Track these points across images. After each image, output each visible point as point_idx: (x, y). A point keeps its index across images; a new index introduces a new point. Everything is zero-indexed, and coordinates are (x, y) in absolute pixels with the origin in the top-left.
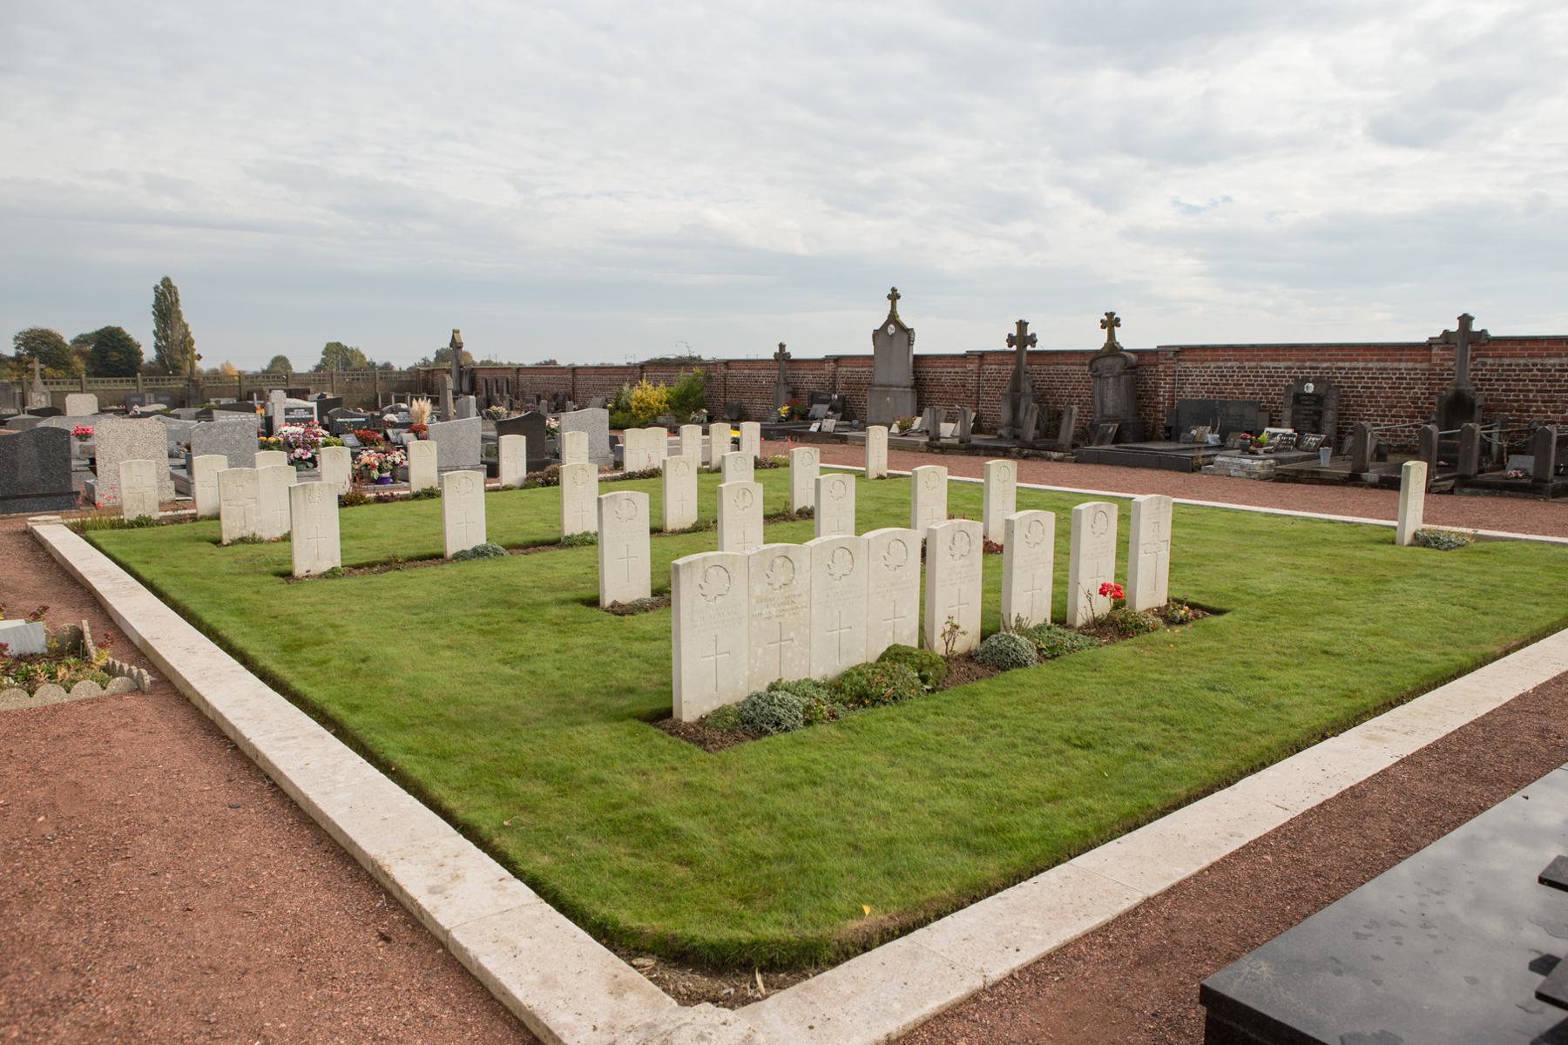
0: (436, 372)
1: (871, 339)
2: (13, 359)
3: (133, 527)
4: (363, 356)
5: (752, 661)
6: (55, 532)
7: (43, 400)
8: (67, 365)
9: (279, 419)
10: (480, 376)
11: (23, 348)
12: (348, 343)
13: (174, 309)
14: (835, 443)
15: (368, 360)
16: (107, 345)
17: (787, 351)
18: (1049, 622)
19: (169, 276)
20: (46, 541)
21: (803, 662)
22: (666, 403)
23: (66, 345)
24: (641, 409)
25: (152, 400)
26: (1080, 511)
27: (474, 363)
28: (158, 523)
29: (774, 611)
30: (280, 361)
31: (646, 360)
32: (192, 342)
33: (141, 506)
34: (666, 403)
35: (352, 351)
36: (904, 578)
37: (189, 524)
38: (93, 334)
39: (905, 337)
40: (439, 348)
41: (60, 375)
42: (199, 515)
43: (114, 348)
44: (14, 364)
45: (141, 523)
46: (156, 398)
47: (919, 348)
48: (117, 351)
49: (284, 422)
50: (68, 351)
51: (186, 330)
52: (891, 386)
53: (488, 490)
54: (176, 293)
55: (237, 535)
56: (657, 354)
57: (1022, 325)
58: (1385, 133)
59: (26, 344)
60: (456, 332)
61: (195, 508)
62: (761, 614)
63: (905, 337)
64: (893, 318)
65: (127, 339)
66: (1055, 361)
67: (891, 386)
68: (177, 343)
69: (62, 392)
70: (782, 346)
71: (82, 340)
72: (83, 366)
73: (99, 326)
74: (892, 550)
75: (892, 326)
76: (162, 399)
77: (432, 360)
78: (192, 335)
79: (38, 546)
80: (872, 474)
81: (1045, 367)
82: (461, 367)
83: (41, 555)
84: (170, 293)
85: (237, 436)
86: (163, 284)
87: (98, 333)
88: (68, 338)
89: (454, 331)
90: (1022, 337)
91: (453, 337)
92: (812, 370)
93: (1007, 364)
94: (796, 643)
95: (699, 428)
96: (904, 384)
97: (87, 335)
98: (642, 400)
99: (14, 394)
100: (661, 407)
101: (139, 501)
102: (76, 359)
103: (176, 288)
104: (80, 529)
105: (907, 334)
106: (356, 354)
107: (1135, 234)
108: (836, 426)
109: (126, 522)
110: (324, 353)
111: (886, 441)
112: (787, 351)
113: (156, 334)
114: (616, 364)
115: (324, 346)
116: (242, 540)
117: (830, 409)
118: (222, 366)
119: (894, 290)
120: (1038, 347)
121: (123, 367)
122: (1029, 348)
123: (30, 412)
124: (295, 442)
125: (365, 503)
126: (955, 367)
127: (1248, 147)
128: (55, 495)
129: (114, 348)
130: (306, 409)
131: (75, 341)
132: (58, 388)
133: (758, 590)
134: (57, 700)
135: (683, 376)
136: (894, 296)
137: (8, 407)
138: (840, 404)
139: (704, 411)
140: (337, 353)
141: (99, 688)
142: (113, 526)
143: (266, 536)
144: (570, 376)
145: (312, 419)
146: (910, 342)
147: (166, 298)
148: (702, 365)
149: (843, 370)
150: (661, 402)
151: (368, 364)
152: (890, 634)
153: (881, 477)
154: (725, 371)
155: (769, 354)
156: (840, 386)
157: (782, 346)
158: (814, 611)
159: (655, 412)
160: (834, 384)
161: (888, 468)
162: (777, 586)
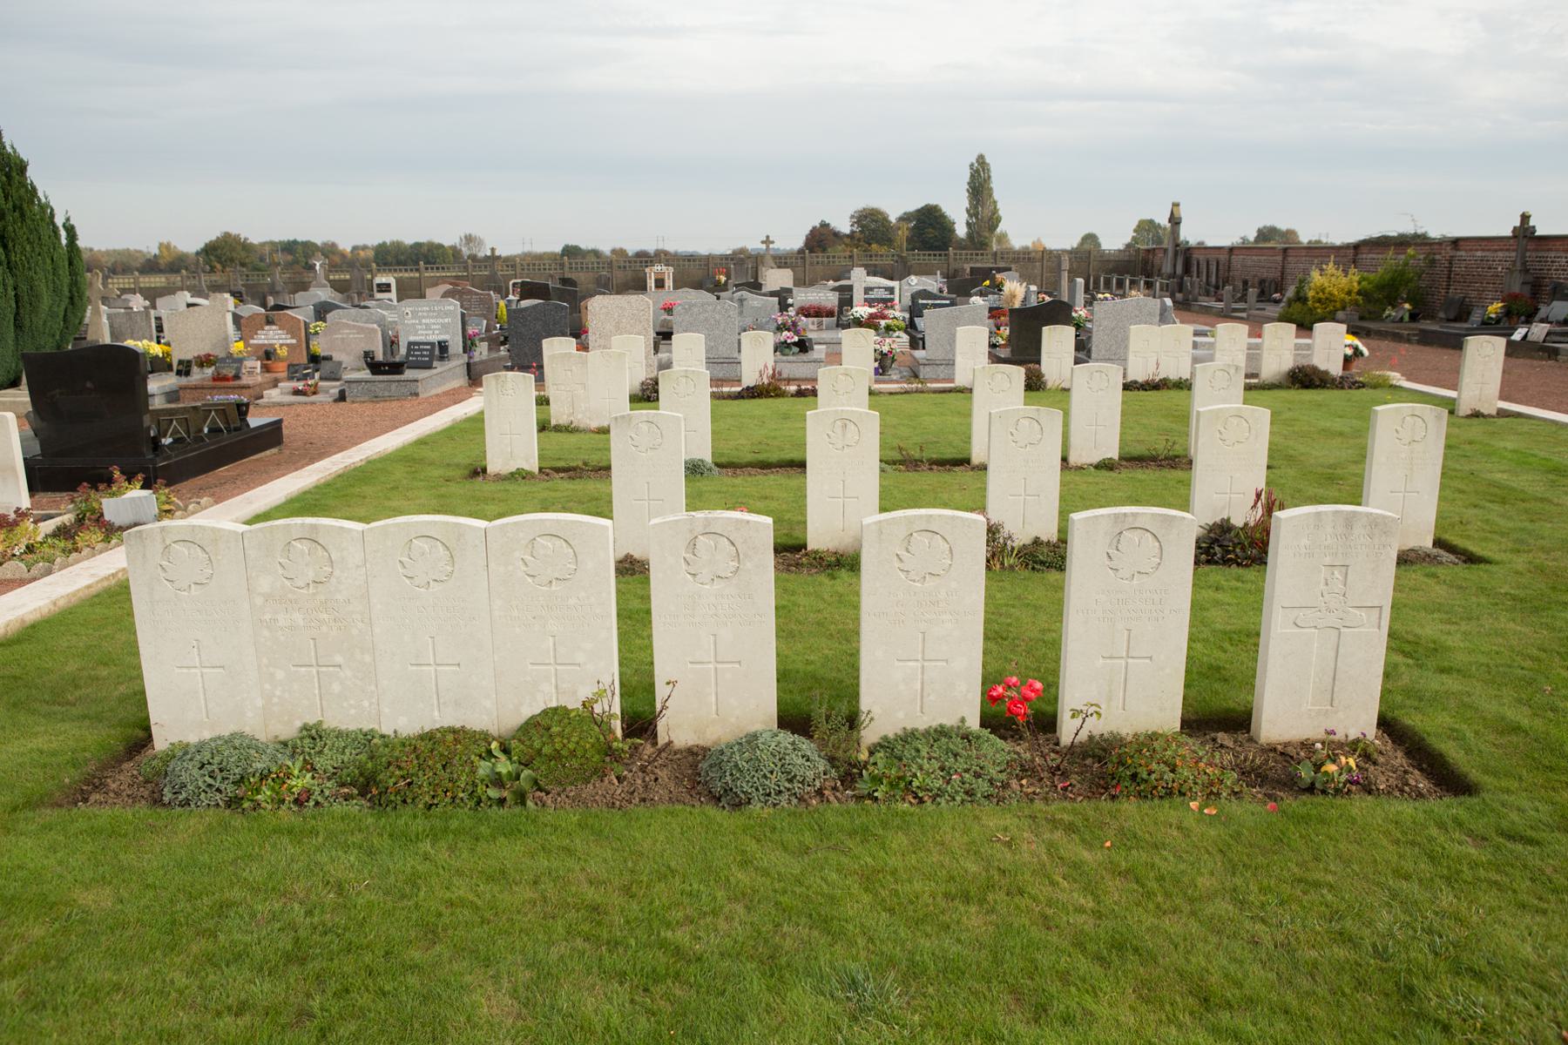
2: (847, 236)
5: (267, 686)
9: (858, 296)
10: (1195, 256)
14: (1542, 359)
17: (1531, 224)
18: (974, 723)
19: (984, 153)
21: (366, 704)
24: (1319, 301)
27: (1299, 242)
30: (1090, 238)
31: (1362, 238)
32: (999, 220)
34: (1359, 293)
36: (572, 602)
40: (1261, 226)
44: (847, 241)
48: (934, 228)
51: (995, 208)
53: (715, 396)
54: (988, 170)
56: (1374, 232)
60: (1176, 205)
62: (276, 620)
65: (943, 216)
68: (986, 219)
70: (1525, 218)
71: (905, 218)
73: (919, 206)
80: (1464, 409)
82: (1177, 245)
85: (717, 317)
86: (977, 161)
87: (918, 211)
97: (910, 213)
98: (1323, 290)
108: (1548, 334)
110: (1135, 231)
112: (1531, 224)
113: (968, 211)
115: (1136, 223)
118: (1033, 243)
130: (887, 289)
131: (901, 219)
133: (264, 584)
135: (1391, 259)
139: (1407, 306)
140: (1149, 230)
143: (1486, 413)
144: (1279, 258)
145: (892, 300)
147: (979, 175)
148: (1426, 244)
150: (1349, 293)
153: (1476, 415)
154: (1452, 253)
155: (1504, 227)
157: (1525, 218)
159: (1338, 305)
161: (1503, 397)
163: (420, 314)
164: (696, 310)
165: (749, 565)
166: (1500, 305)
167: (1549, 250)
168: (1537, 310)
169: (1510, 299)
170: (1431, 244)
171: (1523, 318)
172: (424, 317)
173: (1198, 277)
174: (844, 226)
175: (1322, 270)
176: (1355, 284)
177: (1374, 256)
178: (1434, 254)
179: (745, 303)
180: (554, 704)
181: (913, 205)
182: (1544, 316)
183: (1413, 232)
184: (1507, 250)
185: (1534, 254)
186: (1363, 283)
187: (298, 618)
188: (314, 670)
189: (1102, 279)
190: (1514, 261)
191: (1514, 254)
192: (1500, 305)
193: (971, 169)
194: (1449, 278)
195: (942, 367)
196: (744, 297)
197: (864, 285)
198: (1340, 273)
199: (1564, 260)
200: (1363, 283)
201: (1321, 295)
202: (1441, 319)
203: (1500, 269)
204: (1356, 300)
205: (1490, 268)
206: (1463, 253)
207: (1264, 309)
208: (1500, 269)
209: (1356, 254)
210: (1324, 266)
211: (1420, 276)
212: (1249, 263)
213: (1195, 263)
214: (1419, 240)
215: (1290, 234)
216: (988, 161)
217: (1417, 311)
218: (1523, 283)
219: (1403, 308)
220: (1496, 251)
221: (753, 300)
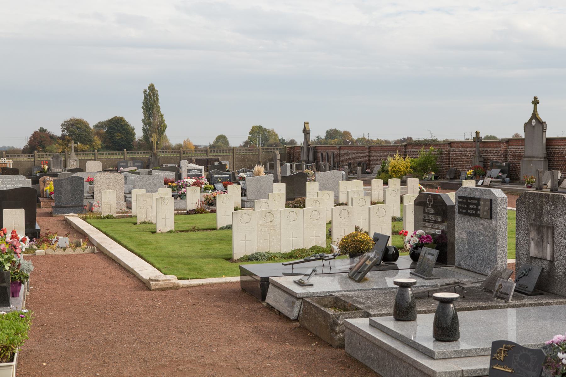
0: (296, 148)
1: (523, 129)
2: (60, 138)
3: (105, 219)
4: (276, 135)
5: (259, 244)
6: (76, 219)
7: (75, 164)
8: (90, 142)
9: (184, 174)
10: (320, 151)
11: (66, 131)
12: (267, 126)
15: (280, 137)
16: (114, 129)
21: (278, 247)
22: (411, 168)
23: (90, 129)
24: (394, 172)
25: (132, 165)
28: (116, 218)
29: (266, 229)
30: (222, 139)
32: (165, 127)
33: (109, 210)
34: (411, 168)
35: (269, 132)
36: (319, 224)
37: (128, 218)
38: (106, 121)
40: (328, 129)
41: (86, 148)
42: (133, 215)
43: (118, 130)
44: (60, 141)
45: (109, 217)
46: (133, 163)
47: (550, 133)
48: (120, 133)
49: (187, 177)
50: (91, 133)
51: (162, 119)
52: (534, 157)
54: (157, 94)
55: (143, 220)
59: (67, 129)
60: (306, 123)
61: (131, 213)
62: (262, 230)
64: (535, 116)
65: (127, 125)
67: (534, 157)
68: (156, 127)
69: (85, 160)
70: (477, 133)
71: (100, 126)
72: (100, 142)
74: (313, 214)
75: (534, 120)
76: (137, 164)
77: (323, 138)
79: (69, 224)
82: (309, 145)
83: (69, 227)
85: (155, 182)
87: (109, 121)
88: (92, 123)
89: (305, 123)
91: (305, 127)
92: (495, 148)
94: (275, 240)
95: (399, 180)
96: (541, 156)
98: (395, 167)
99: (61, 160)
100: (406, 170)
102: (96, 138)
104: (85, 219)
105: (542, 125)
106: (271, 133)
109: (103, 217)
110: (250, 133)
113: (143, 121)
114: (457, 140)
116: (144, 223)
118: (185, 142)
119: (535, 98)
121: (123, 143)
123: (68, 171)
124: (182, 185)
125: (205, 213)
128: (76, 207)
129: (118, 130)
131: (96, 126)
132: (83, 157)
133: (260, 222)
134: (71, 253)
135: (423, 152)
136: (536, 102)
137: (57, 168)
138: (507, 169)
139: (433, 173)
140: (259, 133)
141: (82, 251)
142: (97, 218)
144: (367, 151)
145: (201, 175)
146: (544, 130)
147: (150, 97)
148: (437, 145)
150: (407, 168)
151: (280, 140)
152: (313, 242)
155: (471, 137)
156: (509, 158)
157: (477, 133)
158: (282, 231)
159: (403, 173)
160: (506, 156)
162: (267, 222)
163: (6, 182)
164: (145, 179)
165: (351, 215)
166: (472, 171)
167: (488, 147)
168: (486, 172)
169: (475, 168)
170: (440, 144)
171: (481, 176)
172: (8, 184)
173: (328, 162)
174: (58, 132)
175: (394, 157)
176: (409, 164)
177: (414, 150)
178: (441, 149)
179: (128, 178)
180: (314, 245)
181: (106, 117)
182: (489, 175)
183: (431, 139)
184: (472, 147)
185: (483, 149)
186: (412, 163)
187: (266, 229)
188: (268, 240)
189: (268, 164)
190: (475, 152)
191: (475, 149)
192: (472, 171)
193: (145, 94)
194: (449, 160)
196: (127, 175)
197: (187, 168)
198: (402, 158)
199: (494, 151)
200: (412, 163)
202: (448, 178)
203: (470, 156)
204: (410, 171)
205: (466, 155)
206: (454, 149)
207: (366, 177)
208: (470, 156)
209: (405, 149)
210: (395, 156)
211: (436, 159)
212: (351, 154)
213: (320, 155)
214: (434, 143)
215: (347, 134)
216: (156, 88)
217: (437, 175)
218: (480, 162)
219: (431, 174)
220: (467, 147)
221: (132, 176)
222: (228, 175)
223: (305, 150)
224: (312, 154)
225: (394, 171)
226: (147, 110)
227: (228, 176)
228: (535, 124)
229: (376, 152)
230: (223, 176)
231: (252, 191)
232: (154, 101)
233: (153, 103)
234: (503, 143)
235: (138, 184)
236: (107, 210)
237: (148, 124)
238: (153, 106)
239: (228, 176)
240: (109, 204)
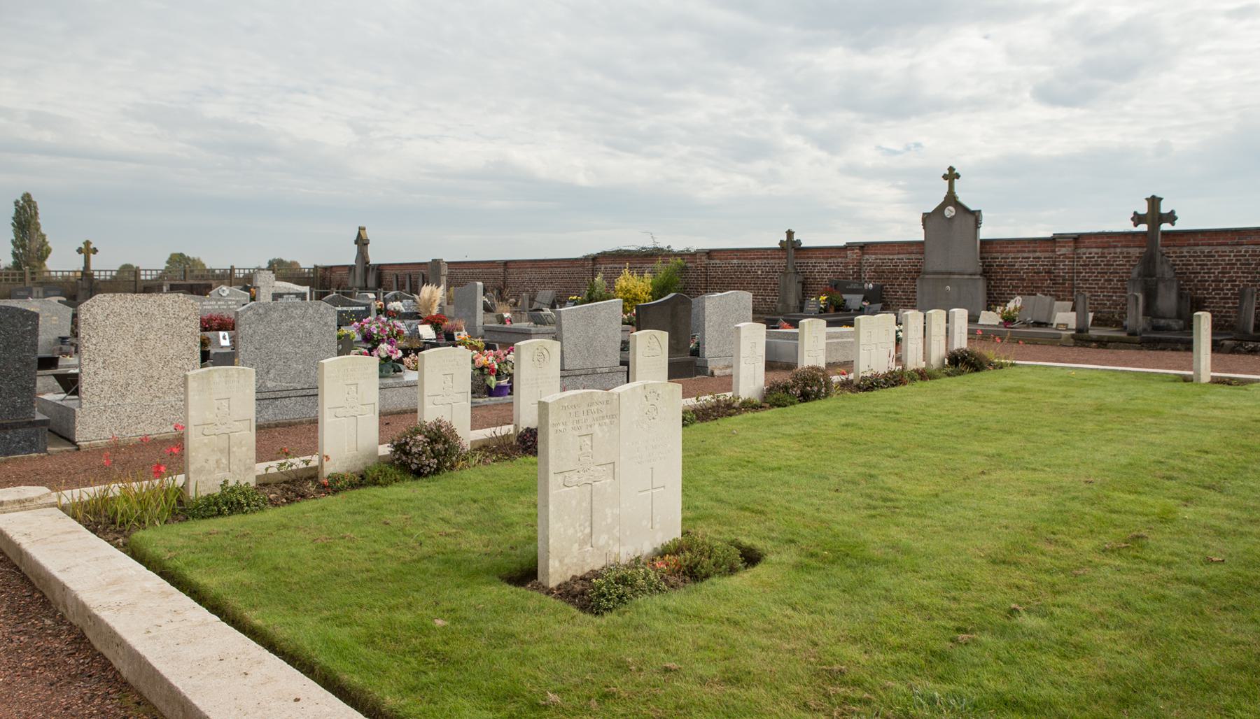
4: (204, 265)
13: (33, 222)
19: (29, 192)
20: (49, 579)
26: (323, 364)
32: (49, 251)
33: (224, 461)
35: (194, 260)
39: (971, 220)
40: (271, 258)
42: (329, 469)
47: (985, 233)
51: (44, 240)
52: (951, 273)
54: (35, 207)
57: (1154, 202)
58: (1047, 95)
60: (362, 229)
63: (971, 220)
66: (1192, 242)
70: (790, 234)
78: (49, 245)
81: (1176, 249)
84: (30, 207)
85: (308, 325)
86: (23, 198)
89: (360, 228)
90: (1154, 213)
91: (359, 234)
93: (1115, 247)
101: (221, 451)
103: (35, 202)
106: (196, 263)
107: (851, 170)
110: (168, 262)
111: (966, 331)
113: (13, 243)
115: (169, 256)
117: (864, 300)
119: (951, 169)
120: (1179, 226)
122: (1165, 227)
126: (1035, 251)
127: (939, 106)
144: (501, 270)
146: (977, 223)
147: (25, 211)
149: (871, 258)
154: (707, 261)
155: (773, 240)
157: (790, 234)
161: (1212, 371)
164: (275, 315)
192: (825, 298)
193: (16, 205)
195: (581, 378)
201: (628, 295)
206: (718, 261)
209: (594, 265)
220: (753, 259)
222: (363, 305)
223: (359, 271)
224: (374, 276)
225: (627, 299)
226: (19, 228)
227: (363, 308)
228: (953, 214)
229: (521, 270)
230: (354, 308)
231: (576, 345)
232: (32, 216)
233: (29, 218)
234: (853, 250)
235: (251, 332)
236: (212, 463)
237: (21, 246)
238: (29, 222)
239: (363, 308)
240: (223, 429)
